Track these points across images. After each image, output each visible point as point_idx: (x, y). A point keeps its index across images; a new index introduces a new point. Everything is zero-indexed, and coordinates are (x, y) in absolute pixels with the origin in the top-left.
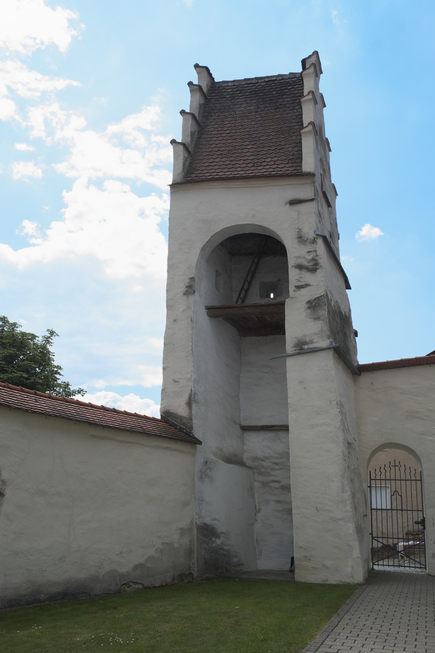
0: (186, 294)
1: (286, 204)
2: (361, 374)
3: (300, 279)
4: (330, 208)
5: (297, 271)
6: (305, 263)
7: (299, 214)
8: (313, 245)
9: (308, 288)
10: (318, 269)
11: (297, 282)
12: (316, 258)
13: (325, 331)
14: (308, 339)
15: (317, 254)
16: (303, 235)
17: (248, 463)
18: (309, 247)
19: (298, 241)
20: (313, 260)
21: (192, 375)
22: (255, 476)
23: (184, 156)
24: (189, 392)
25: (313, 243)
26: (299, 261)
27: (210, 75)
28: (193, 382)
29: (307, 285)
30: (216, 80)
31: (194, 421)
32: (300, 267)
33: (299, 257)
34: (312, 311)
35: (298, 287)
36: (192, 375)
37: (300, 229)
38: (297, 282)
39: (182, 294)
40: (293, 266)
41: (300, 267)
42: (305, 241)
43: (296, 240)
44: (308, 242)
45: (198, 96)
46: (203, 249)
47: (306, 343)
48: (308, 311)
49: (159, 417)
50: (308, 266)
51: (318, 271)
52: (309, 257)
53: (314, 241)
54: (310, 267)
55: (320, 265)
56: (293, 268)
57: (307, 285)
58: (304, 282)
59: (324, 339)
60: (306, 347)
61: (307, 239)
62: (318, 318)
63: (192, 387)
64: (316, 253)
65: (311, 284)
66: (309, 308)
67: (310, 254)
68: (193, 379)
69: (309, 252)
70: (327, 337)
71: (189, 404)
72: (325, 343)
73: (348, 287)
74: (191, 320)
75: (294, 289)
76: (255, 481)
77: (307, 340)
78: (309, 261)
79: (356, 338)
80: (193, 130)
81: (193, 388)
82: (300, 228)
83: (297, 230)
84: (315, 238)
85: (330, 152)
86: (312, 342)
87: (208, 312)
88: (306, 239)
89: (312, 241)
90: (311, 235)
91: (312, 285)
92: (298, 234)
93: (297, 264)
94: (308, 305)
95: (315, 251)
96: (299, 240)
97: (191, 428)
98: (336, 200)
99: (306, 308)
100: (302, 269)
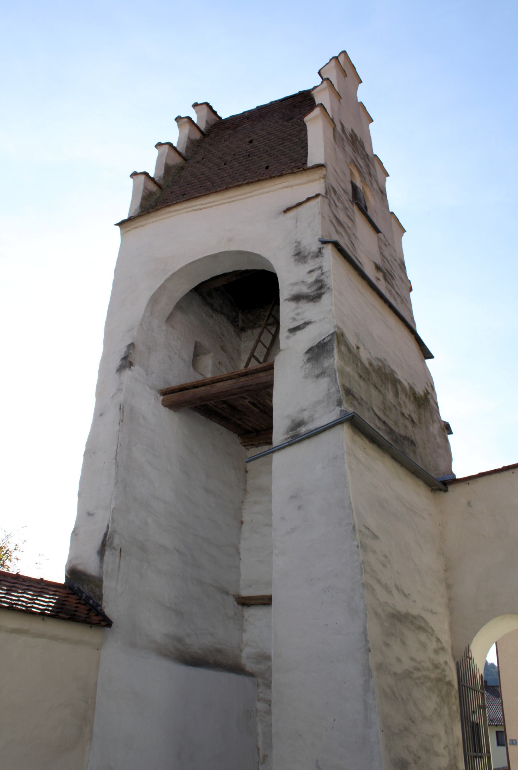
0: (121, 369)
1: (280, 214)
2: (447, 488)
3: (297, 317)
4: (380, 234)
5: (293, 304)
6: (305, 290)
7: (297, 221)
8: (317, 259)
9: (309, 328)
10: (323, 293)
11: (291, 322)
12: (322, 278)
13: (333, 394)
14: (305, 416)
15: (323, 271)
16: (302, 249)
17: (249, 666)
18: (311, 265)
19: (295, 260)
20: (317, 281)
21: (111, 501)
22: (260, 690)
23: (145, 188)
24: (105, 530)
25: (317, 256)
26: (296, 290)
27: (215, 113)
28: (113, 512)
29: (307, 324)
30: (223, 118)
31: (105, 583)
32: (297, 298)
33: (296, 284)
34: (313, 364)
35: (294, 330)
36: (111, 501)
37: (299, 243)
38: (291, 322)
39: (115, 370)
40: (286, 300)
41: (297, 298)
42: (305, 257)
43: (292, 259)
44: (310, 257)
45: (187, 128)
46: (154, 300)
47: (301, 423)
48: (309, 365)
49: (62, 580)
50: (309, 293)
51: (324, 297)
52: (311, 279)
53: (319, 253)
54: (312, 294)
55: (328, 286)
56: (287, 302)
57: (307, 324)
58: (302, 319)
59: (331, 410)
60: (303, 430)
61: (309, 253)
62: (322, 373)
63: (109, 520)
64: (322, 270)
65: (313, 320)
66: (309, 360)
67: (312, 273)
68: (113, 506)
69: (311, 272)
70: (336, 404)
71: (101, 552)
72: (334, 415)
73: (427, 355)
74: (120, 408)
75: (287, 334)
76: (259, 700)
77: (306, 418)
78: (310, 286)
79: (449, 437)
80: (171, 163)
81: (110, 525)
82: (299, 240)
83: (295, 245)
84: (320, 249)
85: (387, 178)
86: (312, 419)
87: (163, 399)
88: (306, 254)
89: (316, 255)
90: (315, 246)
91: (315, 322)
92: (295, 250)
93: (293, 294)
94: (308, 356)
95: (320, 268)
96: (297, 257)
97: (101, 599)
98: (403, 238)
99: (305, 361)
100: (299, 300)
